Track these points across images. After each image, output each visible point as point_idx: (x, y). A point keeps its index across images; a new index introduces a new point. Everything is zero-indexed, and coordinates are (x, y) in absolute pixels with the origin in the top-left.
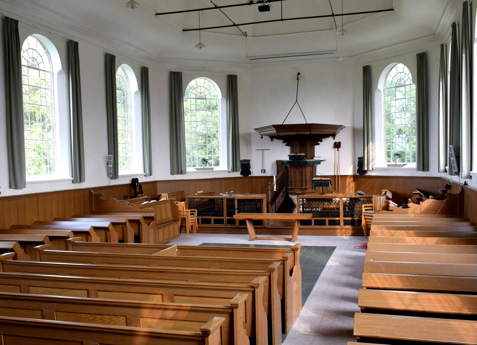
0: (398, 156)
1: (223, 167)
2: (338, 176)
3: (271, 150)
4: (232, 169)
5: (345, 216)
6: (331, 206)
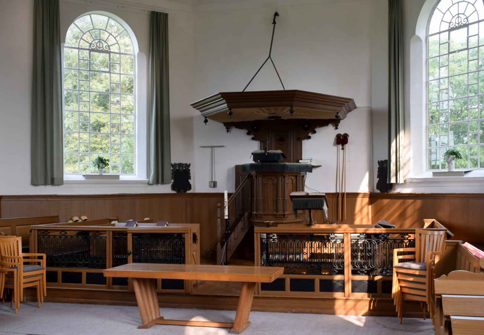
0: (455, 156)
1: (135, 172)
2: (343, 194)
3: (226, 147)
4: (155, 180)
5: (354, 272)
6: (326, 251)
